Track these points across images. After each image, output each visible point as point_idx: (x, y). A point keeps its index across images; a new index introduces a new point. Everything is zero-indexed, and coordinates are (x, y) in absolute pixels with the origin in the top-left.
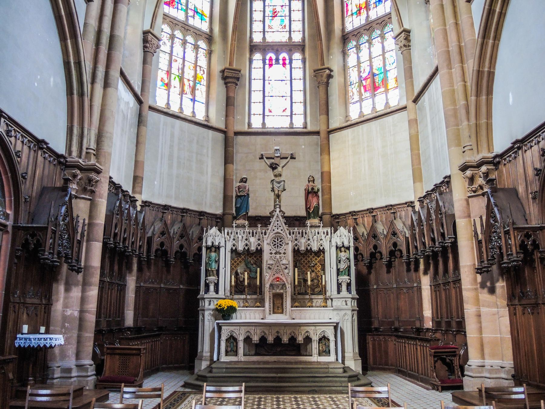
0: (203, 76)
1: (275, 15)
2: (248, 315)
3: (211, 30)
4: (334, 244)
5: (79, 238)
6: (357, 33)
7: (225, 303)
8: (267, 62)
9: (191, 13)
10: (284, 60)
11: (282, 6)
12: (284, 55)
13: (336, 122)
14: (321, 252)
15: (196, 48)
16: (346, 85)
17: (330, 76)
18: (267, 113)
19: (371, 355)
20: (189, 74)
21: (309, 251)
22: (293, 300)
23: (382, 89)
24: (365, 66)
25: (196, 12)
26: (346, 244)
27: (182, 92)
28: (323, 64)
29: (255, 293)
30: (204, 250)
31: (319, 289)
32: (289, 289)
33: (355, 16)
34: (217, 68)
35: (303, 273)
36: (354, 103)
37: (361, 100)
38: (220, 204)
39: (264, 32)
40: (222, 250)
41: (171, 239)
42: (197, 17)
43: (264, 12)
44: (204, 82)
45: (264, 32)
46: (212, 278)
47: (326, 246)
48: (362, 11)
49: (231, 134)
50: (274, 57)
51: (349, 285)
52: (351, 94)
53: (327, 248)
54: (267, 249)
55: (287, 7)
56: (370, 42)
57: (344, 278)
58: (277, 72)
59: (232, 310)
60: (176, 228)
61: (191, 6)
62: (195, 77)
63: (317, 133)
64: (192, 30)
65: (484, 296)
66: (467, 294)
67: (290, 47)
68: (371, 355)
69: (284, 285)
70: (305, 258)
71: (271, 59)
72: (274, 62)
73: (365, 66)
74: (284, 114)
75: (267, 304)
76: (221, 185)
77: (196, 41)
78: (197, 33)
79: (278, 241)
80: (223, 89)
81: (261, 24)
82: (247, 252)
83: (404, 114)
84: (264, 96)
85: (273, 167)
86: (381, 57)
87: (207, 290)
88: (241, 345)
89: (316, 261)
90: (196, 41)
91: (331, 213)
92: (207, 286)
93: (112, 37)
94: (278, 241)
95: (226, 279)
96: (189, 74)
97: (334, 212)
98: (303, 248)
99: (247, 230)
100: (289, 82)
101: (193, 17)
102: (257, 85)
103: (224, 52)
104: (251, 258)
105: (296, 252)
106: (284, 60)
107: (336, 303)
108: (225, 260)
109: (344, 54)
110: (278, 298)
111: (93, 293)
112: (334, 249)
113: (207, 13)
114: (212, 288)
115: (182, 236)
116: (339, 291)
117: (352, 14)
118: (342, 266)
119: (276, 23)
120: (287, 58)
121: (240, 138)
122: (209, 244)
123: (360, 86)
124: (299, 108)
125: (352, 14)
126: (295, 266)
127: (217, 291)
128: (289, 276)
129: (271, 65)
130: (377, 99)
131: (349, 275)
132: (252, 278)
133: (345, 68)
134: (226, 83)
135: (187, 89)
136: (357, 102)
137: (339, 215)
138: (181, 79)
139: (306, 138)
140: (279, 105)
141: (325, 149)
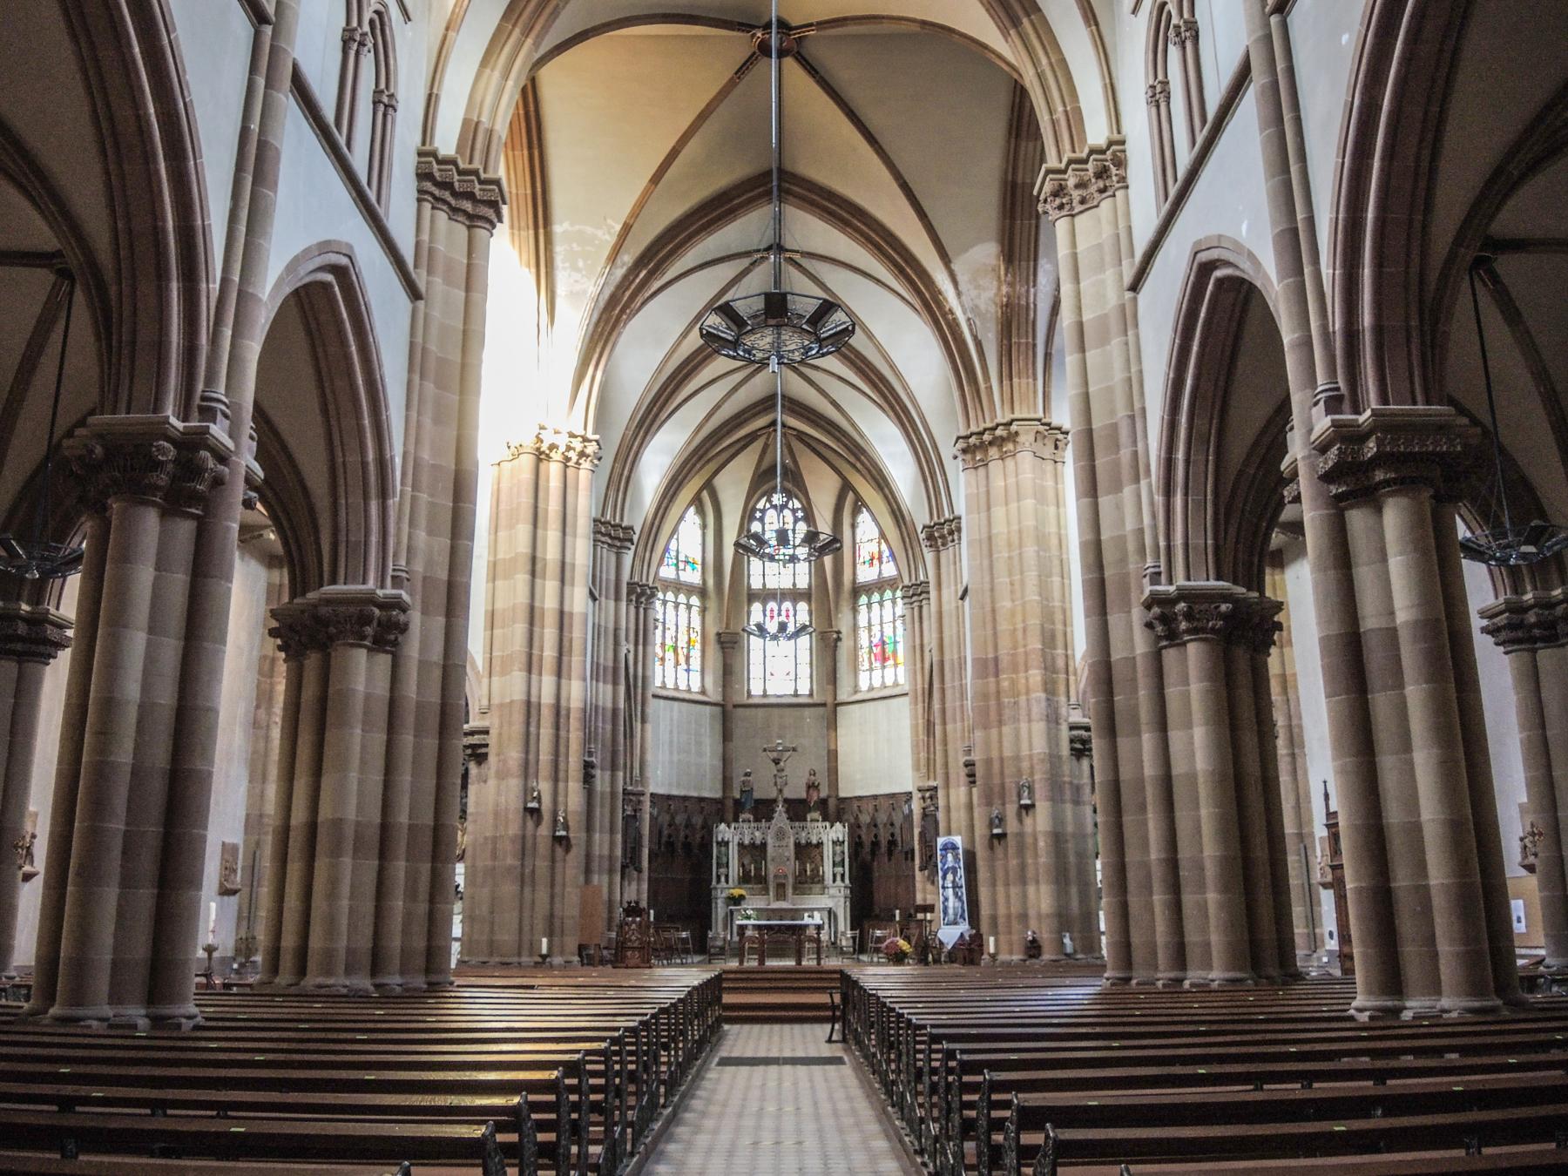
0: (696, 638)
2: (754, 903)
3: (704, 581)
5: (992, 950)
6: (868, 589)
7: (737, 892)
9: (681, 566)
14: (820, 845)
15: (689, 607)
16: (856, 649)
17: (839, 639)
20: (682, 643)
21: (809, 844)
22: (795, 889)
24: (876, 629)
25: (687, 562)
27: (677, 663)
28: (831, 626)
31: (817, 879)
32: (791, 880)
34: (712, 631)
35: (803, 864)
37: (871, 669)
38: (719, 786)
41: (677, 830)
44: (698, 646)
46: (722, 870)
47: (825, 840)
49: (730, 707)
50: (776, 608)
51: (843, 876)
54: (770, 841)
57: (839, 870)
59: (742, 897)
60: (680, 819)
61: (682, 558)
62: (689, 642)
63: (824, 705)
65: (929, 887)
66: (919, 885)
76: (718, 764)
78: (690, 590)
79: (780, 835)
80: (719, 656)
82: (753, 845)
83: (906, 699)
85: (776, 762)
87: (719, 881)
89: (816, 852)
92: (718, 877)
93: (644, 677)
94: (780, 835)
95: (734, 869)
96: (682, 643)
97: (842, 794)
103: (720, 610)
104: (755, 851)
105: (797, 845)
107: (832, 891)
108: (733, 851)
109: (855, 610)
110: (781, 888)
111: (645, 886)
113: (699, 560)
115: (687, 826)
118: (838, 859)
121: (740, 710)
124: (804, 671)
128: (791, 867)
132: (758, 869)
133: (855, 628)
135: (682, 659)
138: (675, 649)
139: (812, 709)
141: (832, 724)
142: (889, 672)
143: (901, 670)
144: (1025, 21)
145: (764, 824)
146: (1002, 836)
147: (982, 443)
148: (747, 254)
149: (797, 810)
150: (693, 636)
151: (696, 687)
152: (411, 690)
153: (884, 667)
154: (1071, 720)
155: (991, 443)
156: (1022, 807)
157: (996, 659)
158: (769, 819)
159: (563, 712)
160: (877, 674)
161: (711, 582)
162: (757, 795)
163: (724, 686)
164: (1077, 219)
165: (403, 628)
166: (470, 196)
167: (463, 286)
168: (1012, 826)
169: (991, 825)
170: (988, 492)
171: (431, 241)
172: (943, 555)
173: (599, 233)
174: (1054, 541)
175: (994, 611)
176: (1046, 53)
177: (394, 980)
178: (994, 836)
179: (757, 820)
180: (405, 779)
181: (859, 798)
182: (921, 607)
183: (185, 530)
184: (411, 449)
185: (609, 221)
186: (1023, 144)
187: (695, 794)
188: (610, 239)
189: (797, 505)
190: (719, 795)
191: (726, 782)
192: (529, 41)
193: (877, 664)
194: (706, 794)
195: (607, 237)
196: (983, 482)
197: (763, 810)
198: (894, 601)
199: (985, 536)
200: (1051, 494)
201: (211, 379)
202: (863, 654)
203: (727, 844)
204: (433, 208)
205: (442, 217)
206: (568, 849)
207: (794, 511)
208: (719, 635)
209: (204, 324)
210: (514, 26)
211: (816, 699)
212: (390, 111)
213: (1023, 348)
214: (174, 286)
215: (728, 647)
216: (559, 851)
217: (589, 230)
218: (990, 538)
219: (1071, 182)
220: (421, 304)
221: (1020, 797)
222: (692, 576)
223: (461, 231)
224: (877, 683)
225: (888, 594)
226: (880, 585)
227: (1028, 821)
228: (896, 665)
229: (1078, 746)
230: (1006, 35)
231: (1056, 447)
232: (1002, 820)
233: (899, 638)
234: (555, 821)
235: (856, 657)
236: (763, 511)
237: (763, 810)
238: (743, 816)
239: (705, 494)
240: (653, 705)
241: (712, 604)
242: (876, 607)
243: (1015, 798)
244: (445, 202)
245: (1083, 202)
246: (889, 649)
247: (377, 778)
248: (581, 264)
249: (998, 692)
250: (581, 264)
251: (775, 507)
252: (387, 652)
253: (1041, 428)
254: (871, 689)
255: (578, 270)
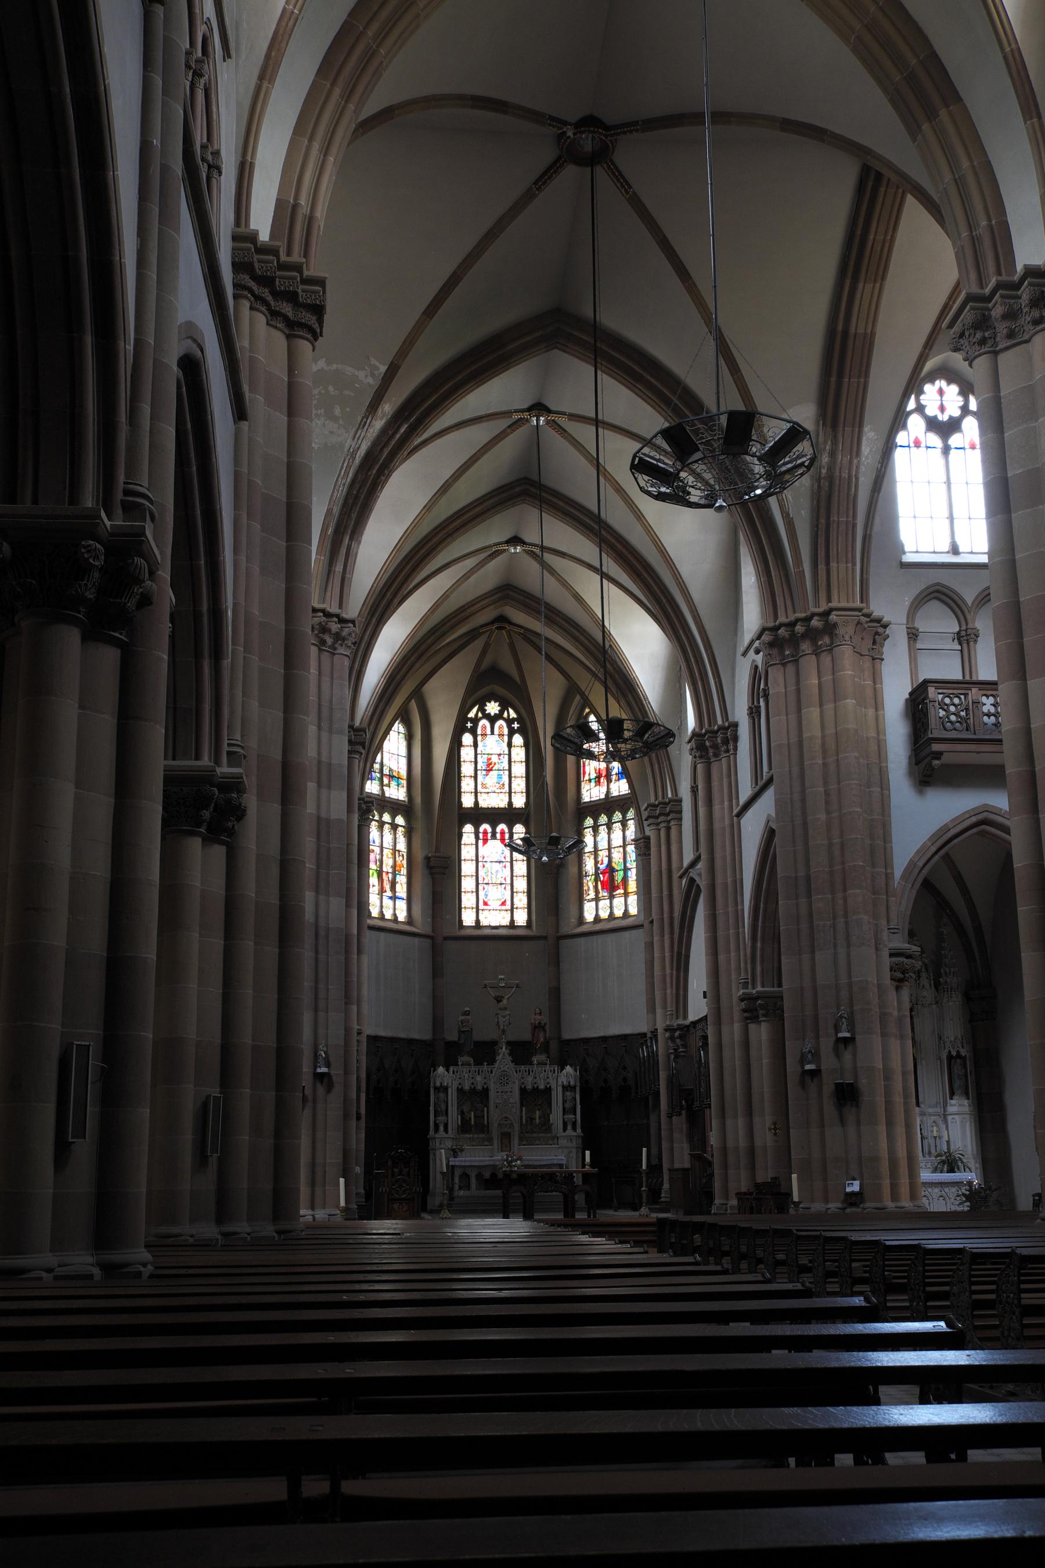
1: (489, 769)
4: (560, 1083)
8: (481, 836)
9: (386, 781)
10: (503, 833)
11: (499, 755)
12: (502, 827)
13: (565, 930)
14: (548, 1090)
15: (394, 827)
18: (481, 906)
19: (230, 629)
20: (387, 866)
21: (536, 1090)
22: (521, 1139)
23: (621, 891)
24: (603, 855)
25: (391, 777)
26: (572, 1083)
27: (382, 891)
29: (482, 1132)
30: (432, 1090)
31: (546, 1125)
32: (517, 1126)
33: (593, 784)
34: (419, 855)
36: (589, 901)
37: (597, 899)
39: (476, 793)
40: (450, 1090)
42: (393, 783)
43: (476, 762)
44: (404, 871)
45: (476, 793)
46: (441, 1118)
48: (602, 780)
50: (489, 830)
51: (574, 1124)
52: (585, 888)
53: (554, 1086)
54: (492, 1087)
55: (507, 757)
56: (609, 826)
58: (494, 850)
61: (386, 771)
62: (394, 866)
63: (545, 938)
64: (389, 805)
67: (508, 815)
68: (230, 629)
69: (512, 1124)
70: (536, 1098)
71: (485, 832)
72: (489, 835)
73: (603, 855)
74: (504, 908)
75: (495, 1142)
77: (393, 818)
81: (472, 782)
82: (473, 1091)
83: (640, 932)
84: (477, 884)
86: (621, 849)
87: (437, 1130)
88: (473, 1180)
90: (393, 818)
91: (559, 1037)
95: (454, 1117)
96: (387, 866)
97: (566, 1036)
98: (529, 1087)
99: (473, 1068)
100: (508, 865)
101: (389, 786)
102: (467, 868)
105: (523, 1091)
106: (503, 833)
107: (563, 1142)
108: (452, 1095)
110: (506, 1136)
112: (560, 1089)
113: (404, 773)
114: (442, 1128)
116: (565, 1130)
117: (590, 780)
118: (568, 1105)
119: (490, 780)
120: (506, 830)
122: (438, 1084)
123: (596, 880)
124: (521, 900)
125: (590, 780)
126: (522, 1105)
127: (446, 1130)
129: (485, 841)
130: (616, 901)
131: (575, 1114)
134: (431, 874)
136: (592, 900)
137: (569, 1041)
140: (495, 895)
141: (555, 960)
142: (619, 902)
143: (633, 900)
144: (943, 113)
145: (485, 1067)
146: (816, 1073)
147: (793, 634)
148: (507, 414)
149: (521, 1052)
150: (399, 859)
151: (402, 916)
152: (249, 889)
153: (611, 897)
154: (892, 945)
155: (804, 636)
156: (839, 1040)
157: (808, 879)
158: (492, 1061)
159: (322, 933)
160: (604, 904)
161: (418, 800)
162: (477, 1036)
163: (434, 917)
164: (1001, 357)
165: (239, 812)
166: (292, 297)
167: (285, 409)
168: (828, 1061)
169: (803, 1061)
170: (798, 691)
171: (251, 350)
172: (715, 767)
173: (361, 374)
174: (873, 747)
175: (805, 824)
176: (968, 154)
177: (242, 1228)
178: (805, 1073)
179: (478, 1063)
180: (247, 992)
181: (586, 1040)
182: (668, 829)
183: (109, 657)
184: (242, 600)
185: (374, 361)
186: (860, 286)
187: (403, 1035)
188: (368, 380)
189: (513, 714)
190: (427, 1036)
191: (437, 1023)
192: (351, 106)
193: (603, 893)
194: (416, 1036)
195: (370, 380)
196: (791, 680)
197: (485, 1053)
198: (624, 824)
199: (794, 739)
200: (869, 693)
201: (132, 469)
202: (589, 883)
203: (446, 1089)
204: (251, 308)
205: (261, 319)
206: (330, 1088)
207: (509, 722)
208: (427, 859)
209: (123, 395)
210: (333, 84)
211: (534, 931)
212: (215, 173)
213: (842, 527)
214: (89, 340)
215: (437, 874)
216: (321, 1089)
217: (349, 370)
218: (800, 743)
219: (997, 312)
220: (244, 425)
221: (837, 1029)
222: (397, 793)
223: (279, 339)
224: (604, 914)
225: (618, 816)
226: (608, 806)
227: (847, 1056)
228: (626, 895)
229: (900, 975)
230: (913, 130)
231: (874, 643)
232: (816, 1055)
233: (632, 864)
234: (316, 1056)
235: (581, 885)
236: (475, 721)
237: (485, 1053)
238: (461, 1060)
239: (413, 705)
240: (369, 936)
241: (419, 825)
242: (603, 830)
243: (832, 1031)
244: (265, 302)
245: (1011, 335)
246: (619, 876)
247: (216, 990)
248: (337, 411)
249: (810, 915)
250: (337, 411)
251: (487, 716)
252: (222, 843)
253: (863, 619)
254: (597, 919)
255: (334, 419)
